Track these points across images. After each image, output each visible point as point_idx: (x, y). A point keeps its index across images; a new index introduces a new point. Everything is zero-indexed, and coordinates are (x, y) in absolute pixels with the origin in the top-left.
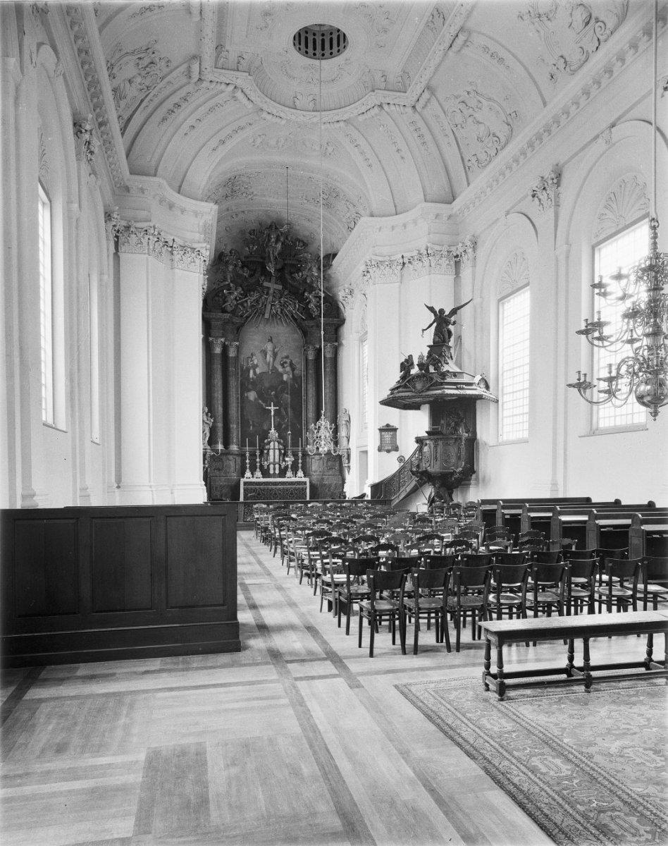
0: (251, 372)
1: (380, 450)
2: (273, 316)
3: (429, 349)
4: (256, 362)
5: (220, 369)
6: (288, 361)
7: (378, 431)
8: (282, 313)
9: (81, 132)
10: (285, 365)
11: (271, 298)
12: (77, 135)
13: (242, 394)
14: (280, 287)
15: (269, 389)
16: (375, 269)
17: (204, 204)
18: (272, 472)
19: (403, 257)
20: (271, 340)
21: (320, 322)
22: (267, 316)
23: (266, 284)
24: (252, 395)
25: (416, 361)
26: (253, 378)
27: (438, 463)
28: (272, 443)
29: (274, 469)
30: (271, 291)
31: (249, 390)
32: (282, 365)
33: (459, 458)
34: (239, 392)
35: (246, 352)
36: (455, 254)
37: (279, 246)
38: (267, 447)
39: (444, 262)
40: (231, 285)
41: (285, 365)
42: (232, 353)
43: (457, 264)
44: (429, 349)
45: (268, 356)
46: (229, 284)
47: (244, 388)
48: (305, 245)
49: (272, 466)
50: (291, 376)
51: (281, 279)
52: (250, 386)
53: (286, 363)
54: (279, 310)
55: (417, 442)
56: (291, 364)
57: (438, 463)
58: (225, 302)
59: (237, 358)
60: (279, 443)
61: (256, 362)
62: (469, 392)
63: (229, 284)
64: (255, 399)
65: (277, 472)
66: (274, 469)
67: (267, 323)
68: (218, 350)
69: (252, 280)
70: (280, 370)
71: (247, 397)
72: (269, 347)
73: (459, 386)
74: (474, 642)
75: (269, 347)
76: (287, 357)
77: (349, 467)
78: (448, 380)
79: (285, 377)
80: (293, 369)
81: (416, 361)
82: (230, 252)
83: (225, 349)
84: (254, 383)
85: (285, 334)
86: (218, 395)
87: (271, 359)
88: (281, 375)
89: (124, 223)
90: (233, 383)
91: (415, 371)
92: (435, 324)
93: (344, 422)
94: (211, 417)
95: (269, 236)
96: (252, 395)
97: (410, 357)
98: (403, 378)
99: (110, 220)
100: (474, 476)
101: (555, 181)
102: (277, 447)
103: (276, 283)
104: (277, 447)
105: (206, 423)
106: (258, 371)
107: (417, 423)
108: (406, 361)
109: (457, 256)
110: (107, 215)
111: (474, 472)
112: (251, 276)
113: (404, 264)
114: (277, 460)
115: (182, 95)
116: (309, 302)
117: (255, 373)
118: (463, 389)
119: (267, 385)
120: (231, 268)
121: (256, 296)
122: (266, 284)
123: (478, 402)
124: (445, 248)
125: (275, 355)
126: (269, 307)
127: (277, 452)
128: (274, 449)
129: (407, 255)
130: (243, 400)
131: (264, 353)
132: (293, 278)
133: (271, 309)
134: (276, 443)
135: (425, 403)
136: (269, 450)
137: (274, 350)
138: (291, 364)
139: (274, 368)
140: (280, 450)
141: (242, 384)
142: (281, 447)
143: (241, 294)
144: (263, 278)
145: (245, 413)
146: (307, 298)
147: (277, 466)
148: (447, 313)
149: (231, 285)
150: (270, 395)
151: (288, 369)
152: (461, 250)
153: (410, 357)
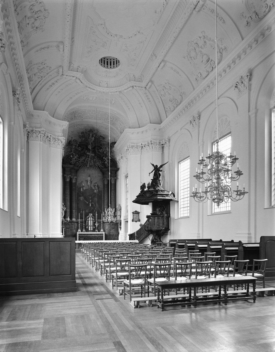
0: (82, 189)
1: (133, 221)
2: (91, 166)
4: (83, 185)
6: (97, 185)
7: (132, 214)
10: (95, 186)
13: (78, 198)
14: (93, 155)
18: (90, 229)
20: (89, 176)
21: (110, 169)
22: (88, 166)
23: (88, 153)
24: (82, 198)
29: (91, 228)
30: (90, 156)
31: (80, 196)
32: (94, 186)
37: (93, 138)
39: (158, 146)
40: (74, 154)
41: (95, 186)
42: (74, 181)
43: (163, 148)
45: (88, 182)
47: (79, 196)
48: (104, 138)
51: (94, 152)
54: (93, 164)
59: (76, 183)
61: (83, 185)
62: (166, 198)
65: (92, 230)
68: (68, 180)
70: (93, 188)
71: (80, 199)
72: (89, 179)
75: (89, 179)
76: (96, 183)
78: (159, 193)
79: (95, 191)
80: (99, 188)
81: (146, 186)
88: (94, 190)
90: (74, 193)
91: (146, 189)
92: (154, 171)
94: (65, 207)
96: (82, 198)
97: (144, 184)
102: (92, 219)
104: (92, 219)
106: (84, 188)
109: (163, 145)
112: (82, 150)
116: (105, 161)
118: (165, 197)
120: (74, 147)
121: (84, 158)
122: (88, 153)
124: (158, 141)
125: (91, 182)
126: (89, 163)
127: (92, 221)
131: (87, 181)
132: (99, 152)
133: (90, 164)
136: (88, 220)
137: (91, 180)
138: (98, 186)
140: (93, 220)
142: (93, 219)
146: (104, 159)
147: (92, 227)
148: (158, 167)
149: (74, 154)
151: (97, 188)
152: (164, 142)
153: (144, 184)
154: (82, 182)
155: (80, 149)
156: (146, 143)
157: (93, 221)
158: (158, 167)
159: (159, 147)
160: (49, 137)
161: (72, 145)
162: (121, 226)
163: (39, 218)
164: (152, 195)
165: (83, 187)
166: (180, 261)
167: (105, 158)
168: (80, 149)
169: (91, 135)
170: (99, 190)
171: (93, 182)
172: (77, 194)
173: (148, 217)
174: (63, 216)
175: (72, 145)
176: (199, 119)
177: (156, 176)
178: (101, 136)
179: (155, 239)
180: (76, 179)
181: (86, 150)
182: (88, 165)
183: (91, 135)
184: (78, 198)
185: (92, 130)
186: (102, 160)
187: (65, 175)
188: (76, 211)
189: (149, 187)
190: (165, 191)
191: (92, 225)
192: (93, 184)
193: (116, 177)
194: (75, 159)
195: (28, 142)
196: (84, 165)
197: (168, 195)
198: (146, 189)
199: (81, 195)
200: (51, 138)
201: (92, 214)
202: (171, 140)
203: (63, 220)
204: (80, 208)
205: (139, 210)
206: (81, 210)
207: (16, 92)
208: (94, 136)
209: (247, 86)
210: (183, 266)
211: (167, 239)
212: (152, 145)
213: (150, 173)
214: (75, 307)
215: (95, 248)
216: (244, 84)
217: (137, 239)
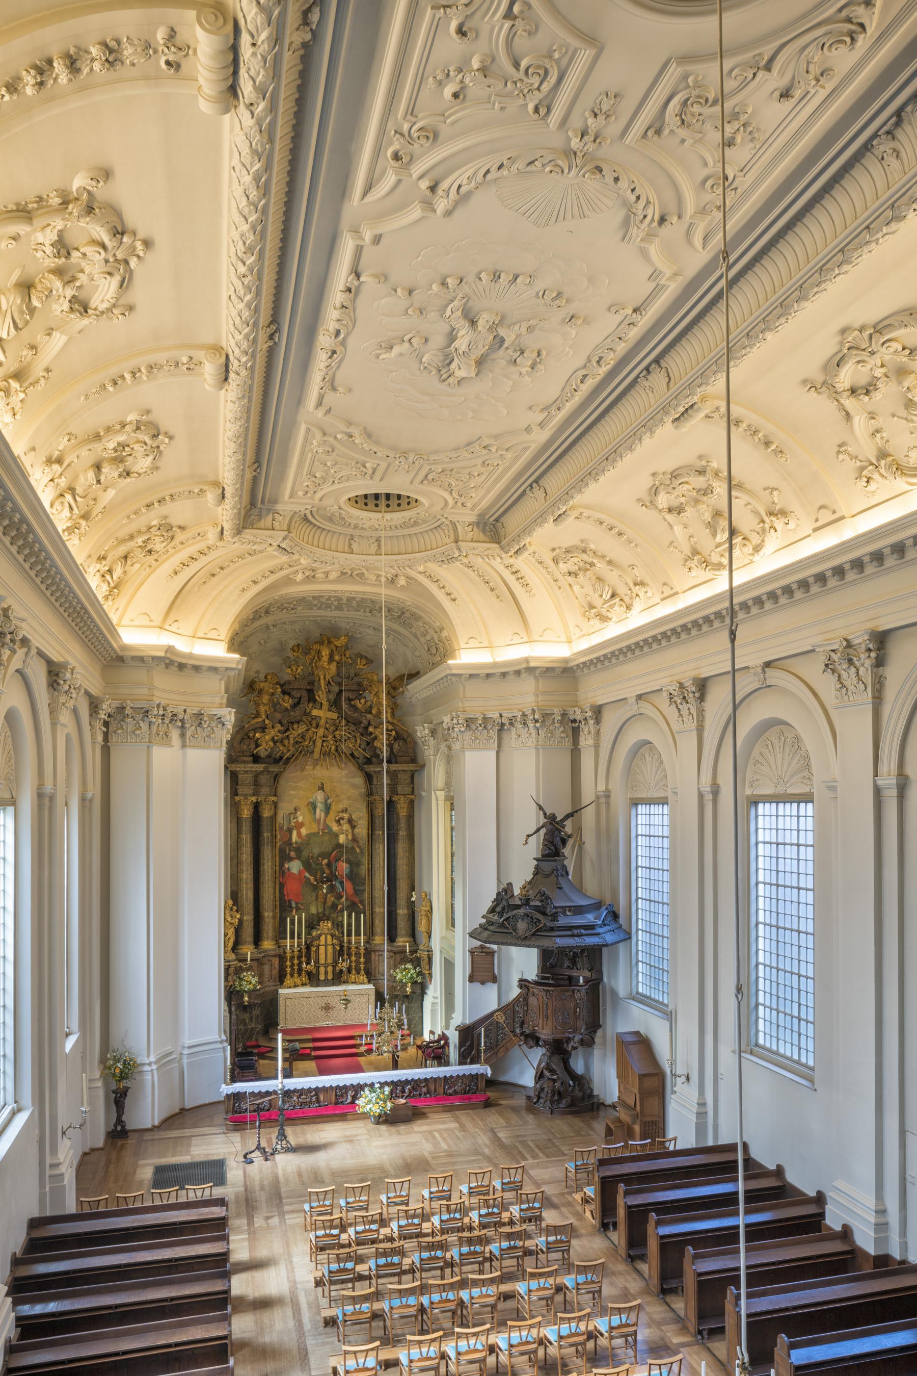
0: (295, 833)
1: (471, 979)
2: (326, 754)
3: (535, 863)
4: (300, 819)
5: (253, 832)
6: (346, 816)
9: (58, 684)
10: (342, 822)
12: (52, 686)
13: (282, 865)
14: (334, 716)
15: (319, 855)
18: (322, 977)
19: (501, 716)
20: (322, 788)
21: (393, 768)
22: (316, 755)
23: (315, 712)
24: (295, 867)
26: (296, 842)
27: (549, 1022)
28: (323, 937)
29: (326, 973)
30: (322, 722)
31: (291, 859)
32: (338, 821)
34: (278, 863)
35: (285, 808)
37: (333, 666)
38: (316, 943)
40: (267, 721)
41: (342, 822)
42: (266, 813)
43: (576, 732)
44: (535, 863)
45: (318, 810)
47: (284, 857)
49: (322, 969)
50: (350, 837)
51: (335, 704)
52: (293, 854)
53: (342, 818)
54: (333, 748)
55: (521, 987)
57: (549, 1022)
59: (273, 818)
60: (333, 936)
61: (300, 819)
64: (300, 872)
65: (330, 977)
67: (317, 764)
68: (246, 813)
69: (296, 714)
70: (335, 828)
71: (288, 869)
72: (320, 796)
75: (320, 796)
77: (430, 975)
78: (563, 921)
79: (342, 839)
82: (266, 677)
83: (257, 807)
84: (298, 850)
85: (343, 782)
86: (247, 875)
87: (323, 815)
88: (337, 836)
89: (116, 704)
90: (267, 853)
92: (543, 831)
93: (423, 913)
94: (237, 911)
96: (295, 867)
99: (97, 712)
101: (697, 695)
102: (330, 942)
104: (330, 942)
106: (304, 831)
107: (522, 962)
108: (505, 890)
110: (93, 705)
111: (599, 1026)
112: (295, 706)
114: (330, 961)
115: (196, 563)
117: (299, 834)
118: (580, 935)
119: (316, 851)
120: (265, 699)
121: (302, 728)
122: (315, 712)
123: (604, 949)
125: (328, 809)
126: (319, 743)
127: (330, 948)
129: (507, 715)
130: (282, 873)
131: (313, 806)
132: (355, 708)
134: (329, 937)
136: (318, 946)
137: (326, 801)
139: (326, 826)
141: (282, 851)
142: (335, 941)
144: (311, 705)
145: (285, 893)
146: (371, 733)
147: (330, 969)
149: (267, 721)
150: (321, 864)
151: (346, 826)
153: (510, 885)
154: (296, 810)
155: (287, 703)
156: (519, 714)
158: (558, 819)
161: (261, 691)
162: (430, 968)
164: (538, 931)
165: (300, 826)
168: (287, 703)
169: (325, 653)
170: (353, 834)
171: (333, 807)
172: (277, 852)
173: (523, 983)
174: (231, 945)
175: (261, 691)
176: (702, 698)
179: (548, 1068)
180: (275, 804)
181: (309, 701)
182: (317, 750)
183: (325, 653)
184: (282, 865)
186: (365, 732)
187: (237, 798)
188: (274, 917)
192: (332, 815)
193: (413, 793)
195: (106, 750)
196: (302, 751)
197: (592, 927)
199: (293, 854)
201: (330, 924)
203: (229, 961)
204: (290, 901)
206: (294, 905)
207: (61, 675)
209: (869, 681)
212: (538, 725)
213: (528, 836)
214: (296, 968)
216: (858, 670)
217: (487, 1061)
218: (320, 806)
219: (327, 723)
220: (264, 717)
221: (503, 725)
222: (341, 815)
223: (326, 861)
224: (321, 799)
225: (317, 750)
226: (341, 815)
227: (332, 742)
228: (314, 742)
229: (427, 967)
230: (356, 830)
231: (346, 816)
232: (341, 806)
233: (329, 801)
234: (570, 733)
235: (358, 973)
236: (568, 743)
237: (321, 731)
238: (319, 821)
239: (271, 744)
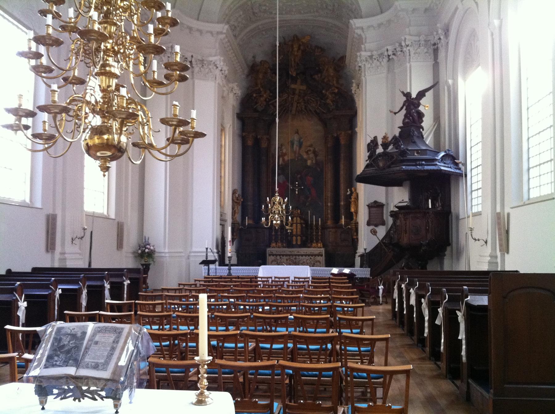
3: (400, 130)
6: (312, 149)
7: (367, 207)
8: (306, 109)
10: (309, 152)
11: (296, 97)
14: (304, 87)
16: (364, 63)
17: (216, 25)
18: (294, 243)
20: (297, 132)
22: (294, 112)
23: (293, 86)
25: (380, 142)
29: (297, 240)
30: (297, 92)
32: (307, 153)
33: (427, 231)
36: (432, 43)
37: (300, 53)
39: (423, 49)
41: (309, 152)
43: (436, 52)
44: (400, 130)
45: (295, 146)
46: (259, 89)
48: (322, 50)
50: (314, 162)
53: (310, 150)
54: (303, 107)
56: (314, 152)
58: (256, 103)
62: (426, 168)
63: (259, 89)
65: (299, 243)
66: (297, 240)
70: (305, 157)
72: (296, 137)
73: (418, 163)
74: (16, 367)
75: (296, 137)
76: (311, 146)
79: (309, 163)
81: (380, 142)
87: (298, 148)
88: (306, 161)
91: (380, 150)
92: (405, 108)
95: (292, 46)
97: (375, 138)
98: (370, 157)
100: (449, 248)
102: (299, 222)
103: (301, 85)
104: (299, 222)
105: (236, 202)
109: (434, 44)
113: (389, 56)
116: (327, 98)
118: (422, 165)
122: (293, 86)
124: (422, 38)
126: (295, 105)
128: (297, 223)
133: (297, 106)
134: (298, 218)
135: (406, 180)
137: (300, 140)
139: (300, 155)
140: (301, 224)
142: (302, 221)
143: (270, 96)
147: (299, 238)
148: (414, 95)
149: (262, 89)
151: (312, 155)
152: (437, 38)
153: (375, 138)
157: (302, 226)
158: (414, 95)
159: (425, 50)
160: (189, 59)
163: (163, 211)
166: (278, 301)
167: (326, 91)
170: (316, 160)
177: (409, 119)
178: (317, 47)
182: (294, 109)
185: (297, 37)
189: (385, 145)
190: (428, 151)
191: (299, 233)
192: (303, 149)
194: (265, 100)
198: (380, 150)
200: (193, 60)
201: (299, 211)
202: (494, 34)
205: (382, 200)
208: (302, 48)
210: (247, 307)
211: (432, 267)
215: (342, 287)
218: (296, 143)
219: (300, 92)
220: (259, 86)
221: (389, 56)
222: (309, 148)
223: (299, 176)
224: (294, 138)
225: (294, 109)
226: (309, 148)
227: (302, 104)
228: (292, 104)
229: (355, 234)
230: (318, 158)
231: (312, 149)
232: (309, 143)
233: (302, 140)
234: (432, 52)
235: (317, 242)
236: (431, 63)
237: (296, 97)
238: (295, 152)
239: (265, 103)
